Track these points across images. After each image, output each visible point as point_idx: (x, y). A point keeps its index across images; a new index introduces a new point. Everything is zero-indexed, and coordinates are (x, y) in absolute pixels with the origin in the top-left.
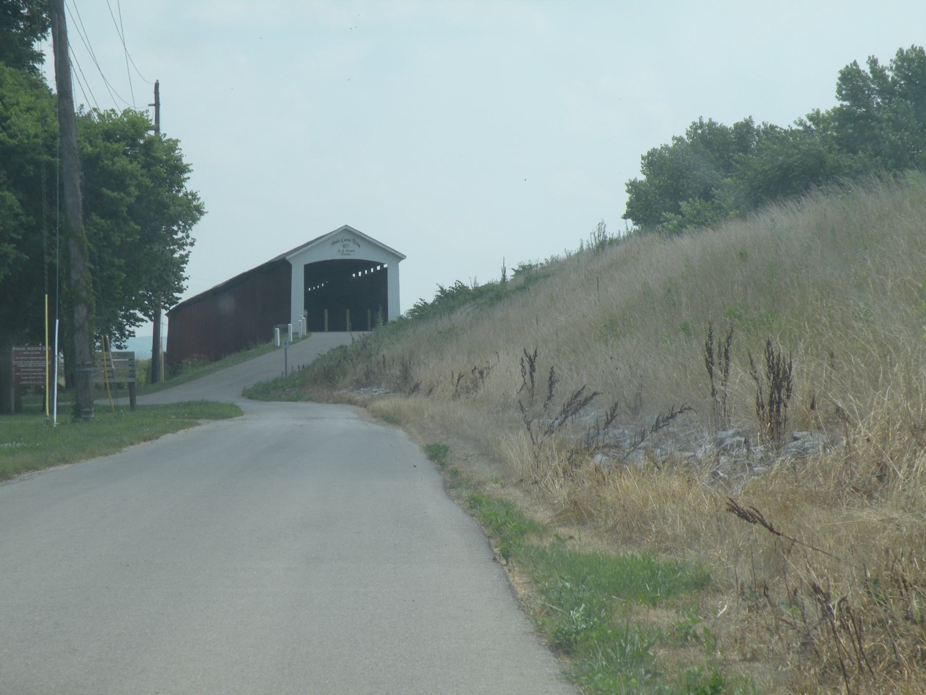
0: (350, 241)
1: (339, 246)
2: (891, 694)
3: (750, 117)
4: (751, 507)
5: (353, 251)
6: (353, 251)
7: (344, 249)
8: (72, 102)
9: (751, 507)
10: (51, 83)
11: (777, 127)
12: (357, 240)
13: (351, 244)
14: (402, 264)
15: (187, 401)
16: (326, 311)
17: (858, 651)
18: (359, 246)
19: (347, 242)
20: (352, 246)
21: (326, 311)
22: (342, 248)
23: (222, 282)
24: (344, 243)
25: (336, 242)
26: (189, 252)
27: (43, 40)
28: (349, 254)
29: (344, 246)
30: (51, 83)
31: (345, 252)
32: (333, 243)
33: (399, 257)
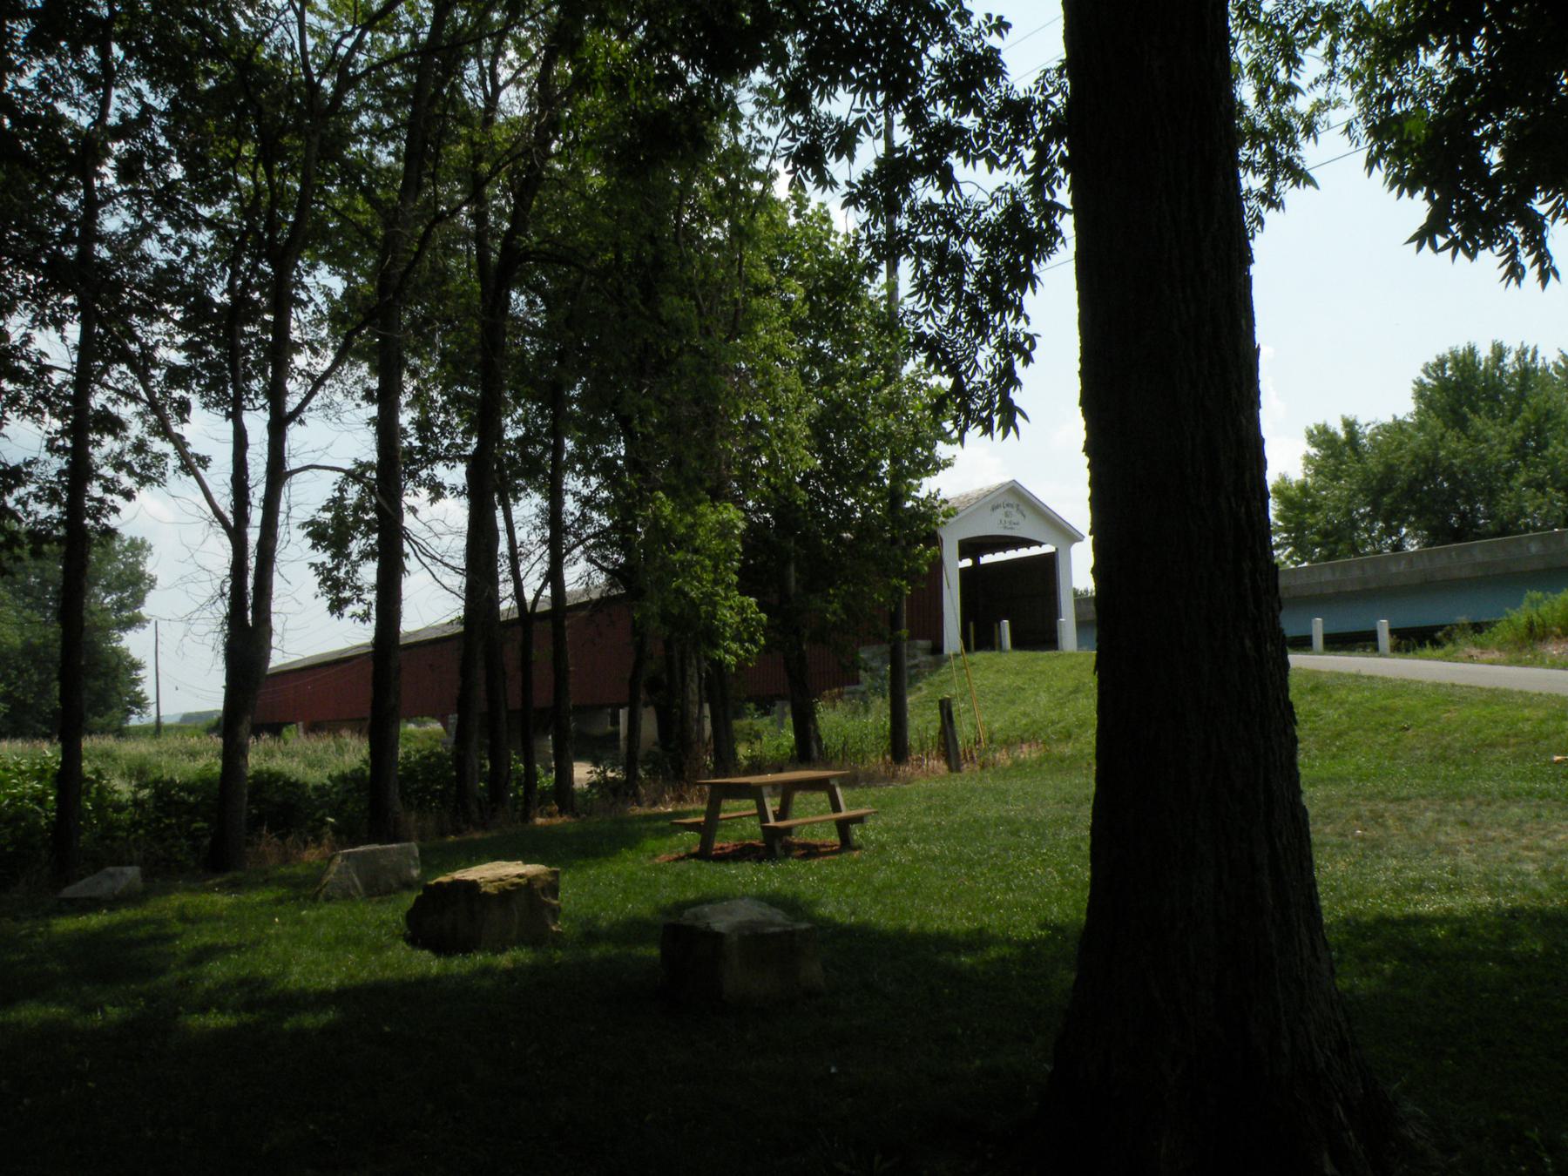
0: (1012, 506)
1: (1000, 512)
13: (1014, 511)
20: (1016, 517)
25: (997, 507)
29: (1007, 515)
32: (994, 508)
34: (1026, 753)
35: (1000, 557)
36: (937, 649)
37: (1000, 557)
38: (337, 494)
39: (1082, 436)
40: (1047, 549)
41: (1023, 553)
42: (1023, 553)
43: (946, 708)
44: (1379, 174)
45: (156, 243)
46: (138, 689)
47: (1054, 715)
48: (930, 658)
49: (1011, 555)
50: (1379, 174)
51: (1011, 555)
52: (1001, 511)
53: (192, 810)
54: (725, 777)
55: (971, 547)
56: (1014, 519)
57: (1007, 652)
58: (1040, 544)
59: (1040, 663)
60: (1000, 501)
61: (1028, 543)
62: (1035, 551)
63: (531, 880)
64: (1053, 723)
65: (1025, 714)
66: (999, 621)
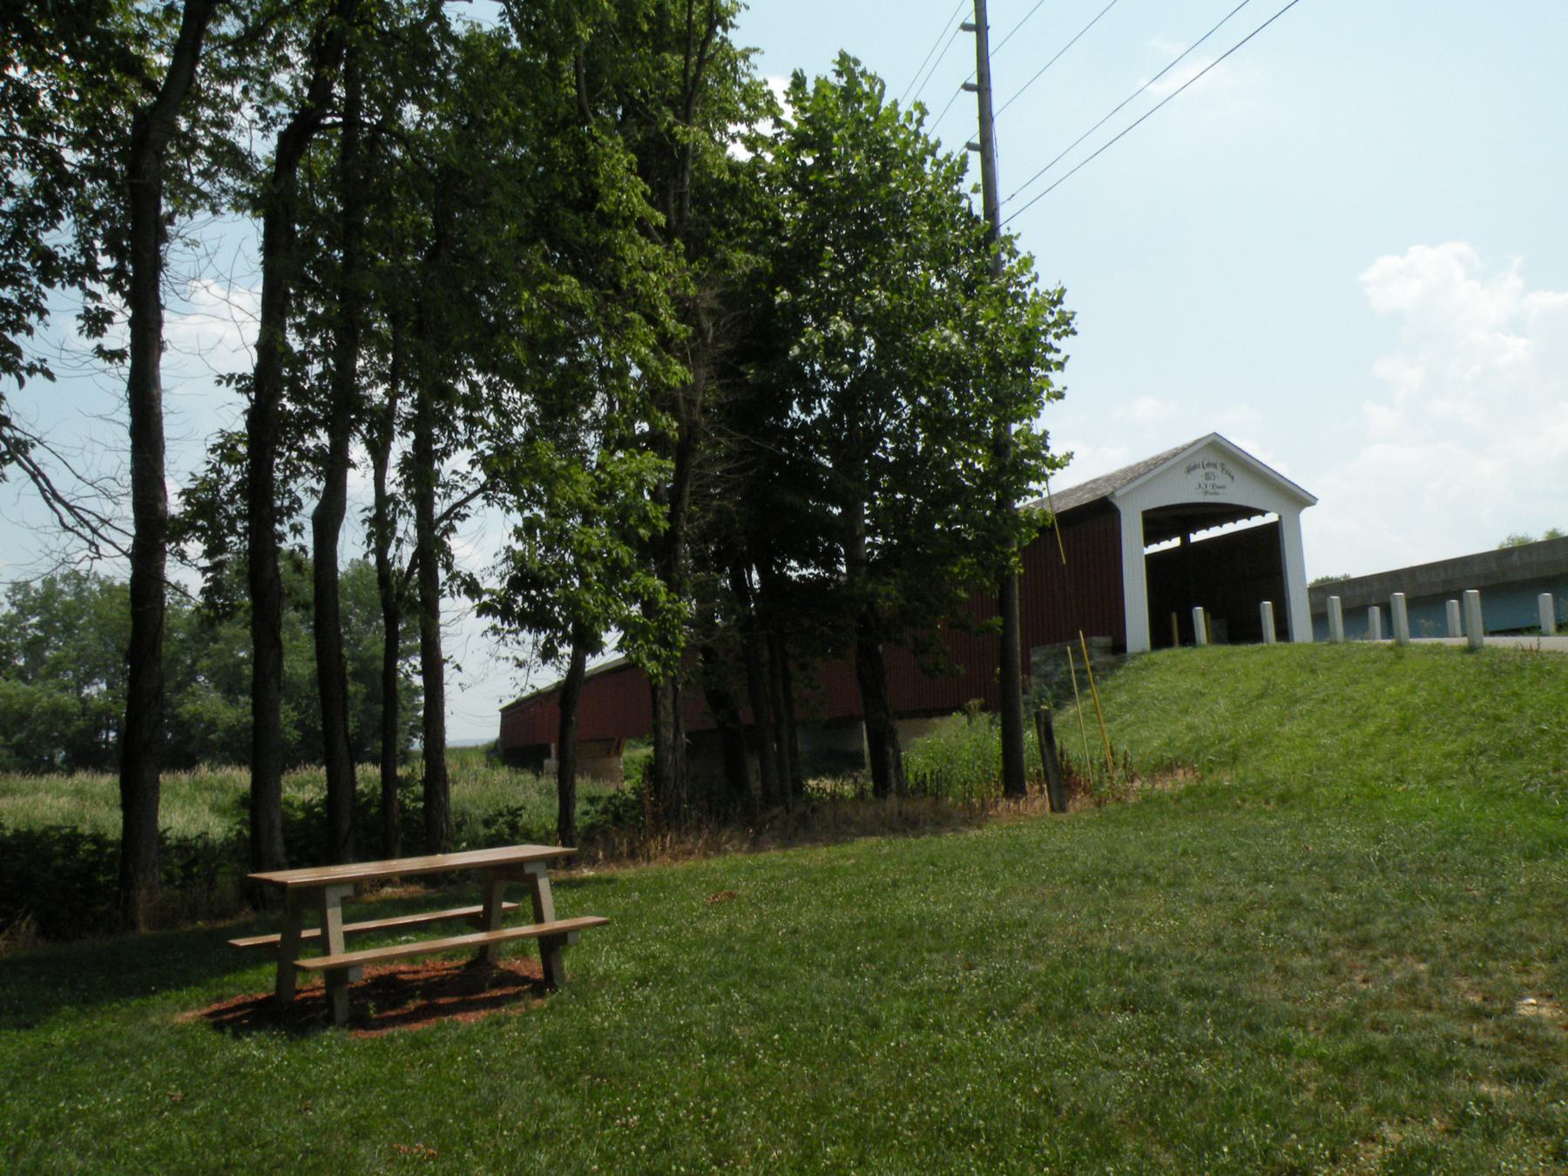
0: (1215, 466)
1: (1199, 474)
3: (845, 64)
4: (364, 510)
5: (1223, 487)
6: (1223, 487)
9: (364, 510)
11: (857, 63)
12: (1229, 467)
13: (1218, 472)
14: (1306, 515)
16: (1174, 616)
17: (433, 893)
19: (1212, 470)
20: (1221, 479)
21: (1174, 616)
24: (1207, 470)
25: (1195, 467)
26: (1067, 357)
27: (1066, 306)
28: (1217, 494)
29: (1207, 476)
32: (1190, 470)
35: (1215, 532)
36: (1119, 647)
37: (1215, 532)
38: (229, 1031)
40: (1271, 518)
41: (1243, 525)
42: (1243, 525)
45: (15, 172)
47: (1225, 729)
48: (1111, 659)
49: (1229, 528)
51: (1229, 528)
52: (1200, 472)
53: (453, 39)
54: (431, 850)
55: (1158, 523)
56: (1218, 482)
57: (1203, 646)
58: (1263, 513)
60: (1198, 460)
61: (1248, 512)
62: (1257, 521)
63: (254, 872)
64: (1222, 739)
65: (1191, 728)
66: (1259, 601)
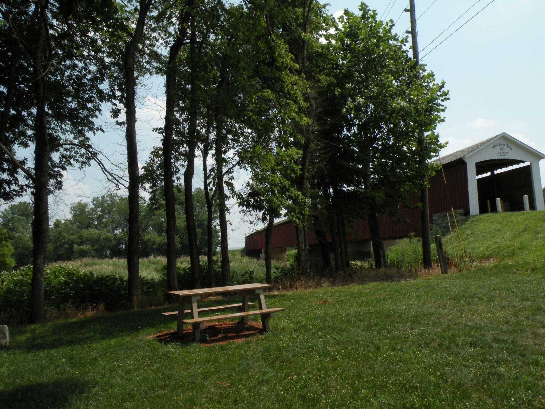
0: (504, 145)
1: (498, 149)
2: (2, 89)
3: (363, 7)
5: (508, 153)
6: (508, 153)
7: (502, 151)
8: (191, 188)
10: (410, 54)
13: (505, 147)
15: (23, 201)
16: (489, 201)
18: (511, 149)
19: (503, 146)
20: (507, 150)
22: (500, 151)
23: (533, 169)
24: (501, 146)
25: (496, 146)
29: (501, 149)
30: (410, 54)
31: (502, 154)
32: (494, 147)
33: (538, 156)
34: (492, 262)
35: (504, 170)
36: (467, 213)
37: (504, 170)
39: (136, 123)
40: (527, 164)
42: (516, 167)
43: (247, 170)
44: (428, 70)
46: (63, 222)
47: (509, 243)
48: (464, 218)
50: (428, 70)
51: (510, 168)
57: (500, 213)
58: (524, 162)
59: (513, 217)
61: (517, 162)
62: (521, 165)
65: (495, 243)
